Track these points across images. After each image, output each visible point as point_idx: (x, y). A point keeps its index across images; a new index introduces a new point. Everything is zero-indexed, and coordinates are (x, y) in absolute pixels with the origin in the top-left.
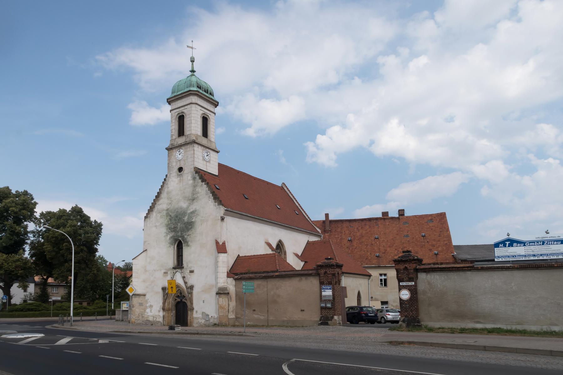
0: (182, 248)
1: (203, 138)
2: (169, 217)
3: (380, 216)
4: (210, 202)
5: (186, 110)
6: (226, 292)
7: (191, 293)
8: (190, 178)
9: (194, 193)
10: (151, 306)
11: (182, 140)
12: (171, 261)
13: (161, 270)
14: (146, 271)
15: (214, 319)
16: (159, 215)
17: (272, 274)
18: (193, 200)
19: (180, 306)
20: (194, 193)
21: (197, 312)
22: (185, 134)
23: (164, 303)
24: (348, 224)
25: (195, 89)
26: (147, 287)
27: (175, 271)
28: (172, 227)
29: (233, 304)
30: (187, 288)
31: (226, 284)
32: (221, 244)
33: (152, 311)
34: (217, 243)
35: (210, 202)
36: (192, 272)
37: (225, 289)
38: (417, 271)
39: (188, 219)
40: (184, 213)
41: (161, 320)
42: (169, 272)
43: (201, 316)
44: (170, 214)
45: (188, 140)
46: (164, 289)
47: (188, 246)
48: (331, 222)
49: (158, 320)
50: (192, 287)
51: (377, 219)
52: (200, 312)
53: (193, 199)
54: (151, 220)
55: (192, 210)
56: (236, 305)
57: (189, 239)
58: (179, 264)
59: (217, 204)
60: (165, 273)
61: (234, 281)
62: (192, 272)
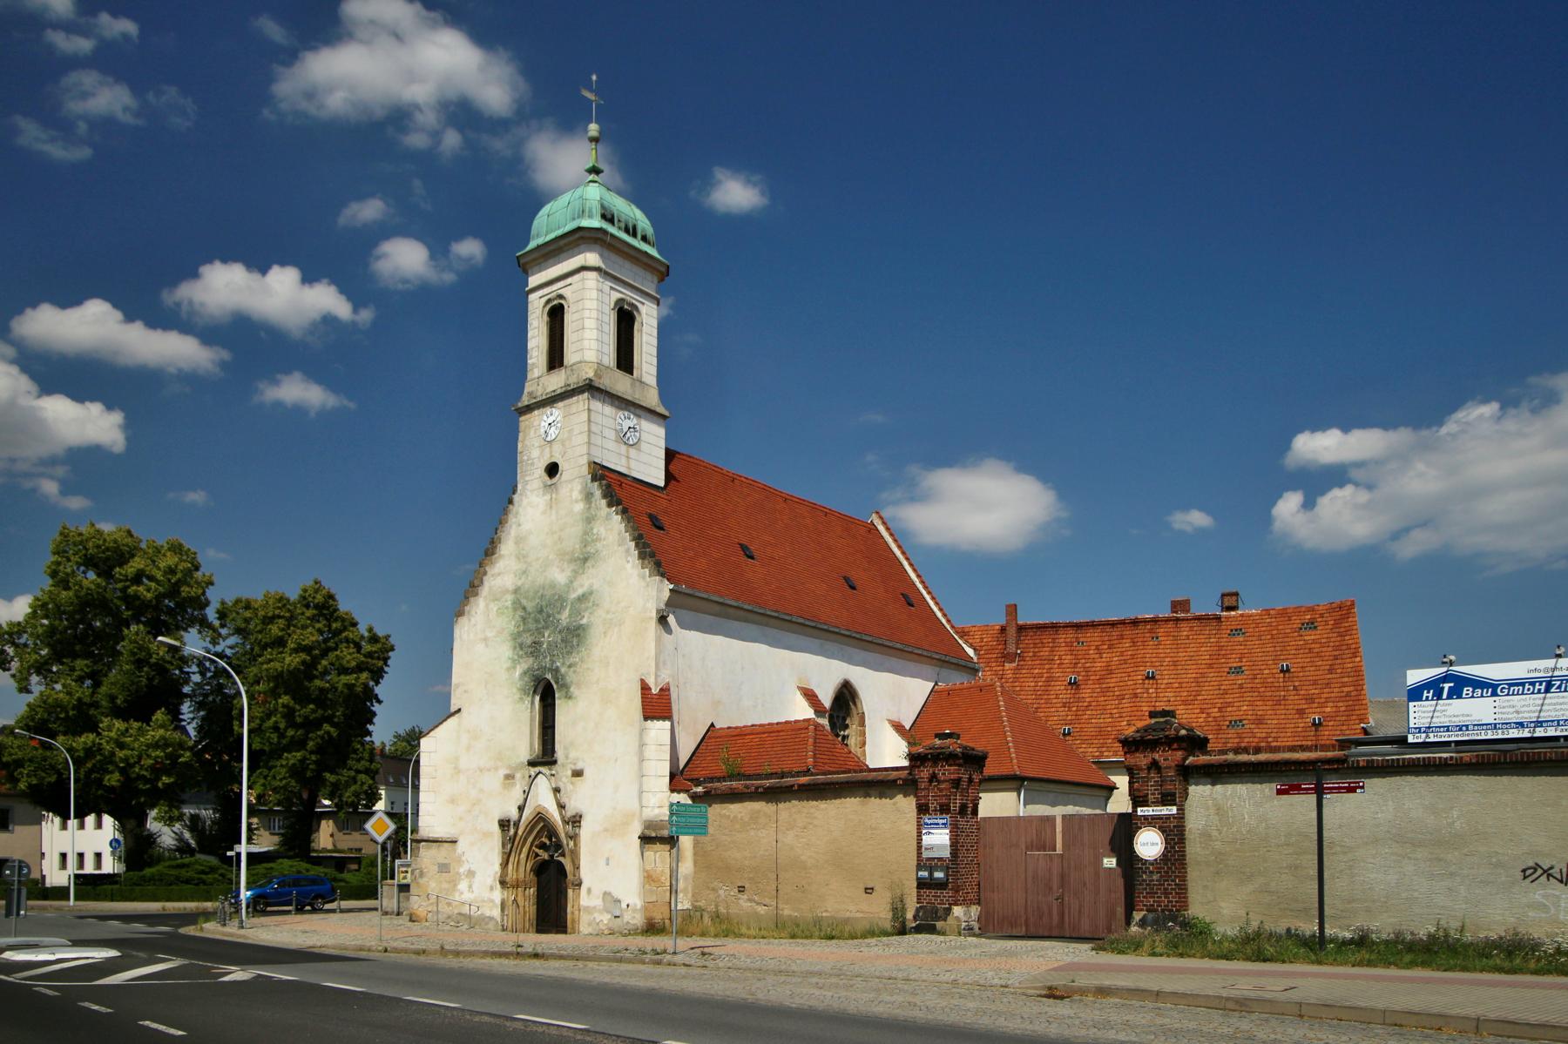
1: (620, 374)
4: (629, 566)
7: (574, 837)
8: (576, 494)
9: (587, 539)
10: (471, 874)
12: (525, 744)
13: (496, 769)
14: (457, 771)
15: (635, 911)
16: (494, 607)
18: (585, 560)
19: (545, 868)
20: (587, 539)
21: (589, 891)
22: (565, 362)
23: (505, 864)
24: (1071, 635)
25: (596, 223)
27: (533, 771)
28: (529, 641)
30: (566, 822)
32: (655, 691)
34: (645, 688)
35: (629, 566)
36: (578, 774)
38: (1188, 774)
42: (518, 776)
44: (524, 602)
46: (504, 824)
47: (569, 697)
48: (1021, 629)
50: (576, 820)
51: (1155, 621)
53: (584, 560)
55: (580, 591)
57: (571, 677)
58: (546, 756)
62: (578, 774)
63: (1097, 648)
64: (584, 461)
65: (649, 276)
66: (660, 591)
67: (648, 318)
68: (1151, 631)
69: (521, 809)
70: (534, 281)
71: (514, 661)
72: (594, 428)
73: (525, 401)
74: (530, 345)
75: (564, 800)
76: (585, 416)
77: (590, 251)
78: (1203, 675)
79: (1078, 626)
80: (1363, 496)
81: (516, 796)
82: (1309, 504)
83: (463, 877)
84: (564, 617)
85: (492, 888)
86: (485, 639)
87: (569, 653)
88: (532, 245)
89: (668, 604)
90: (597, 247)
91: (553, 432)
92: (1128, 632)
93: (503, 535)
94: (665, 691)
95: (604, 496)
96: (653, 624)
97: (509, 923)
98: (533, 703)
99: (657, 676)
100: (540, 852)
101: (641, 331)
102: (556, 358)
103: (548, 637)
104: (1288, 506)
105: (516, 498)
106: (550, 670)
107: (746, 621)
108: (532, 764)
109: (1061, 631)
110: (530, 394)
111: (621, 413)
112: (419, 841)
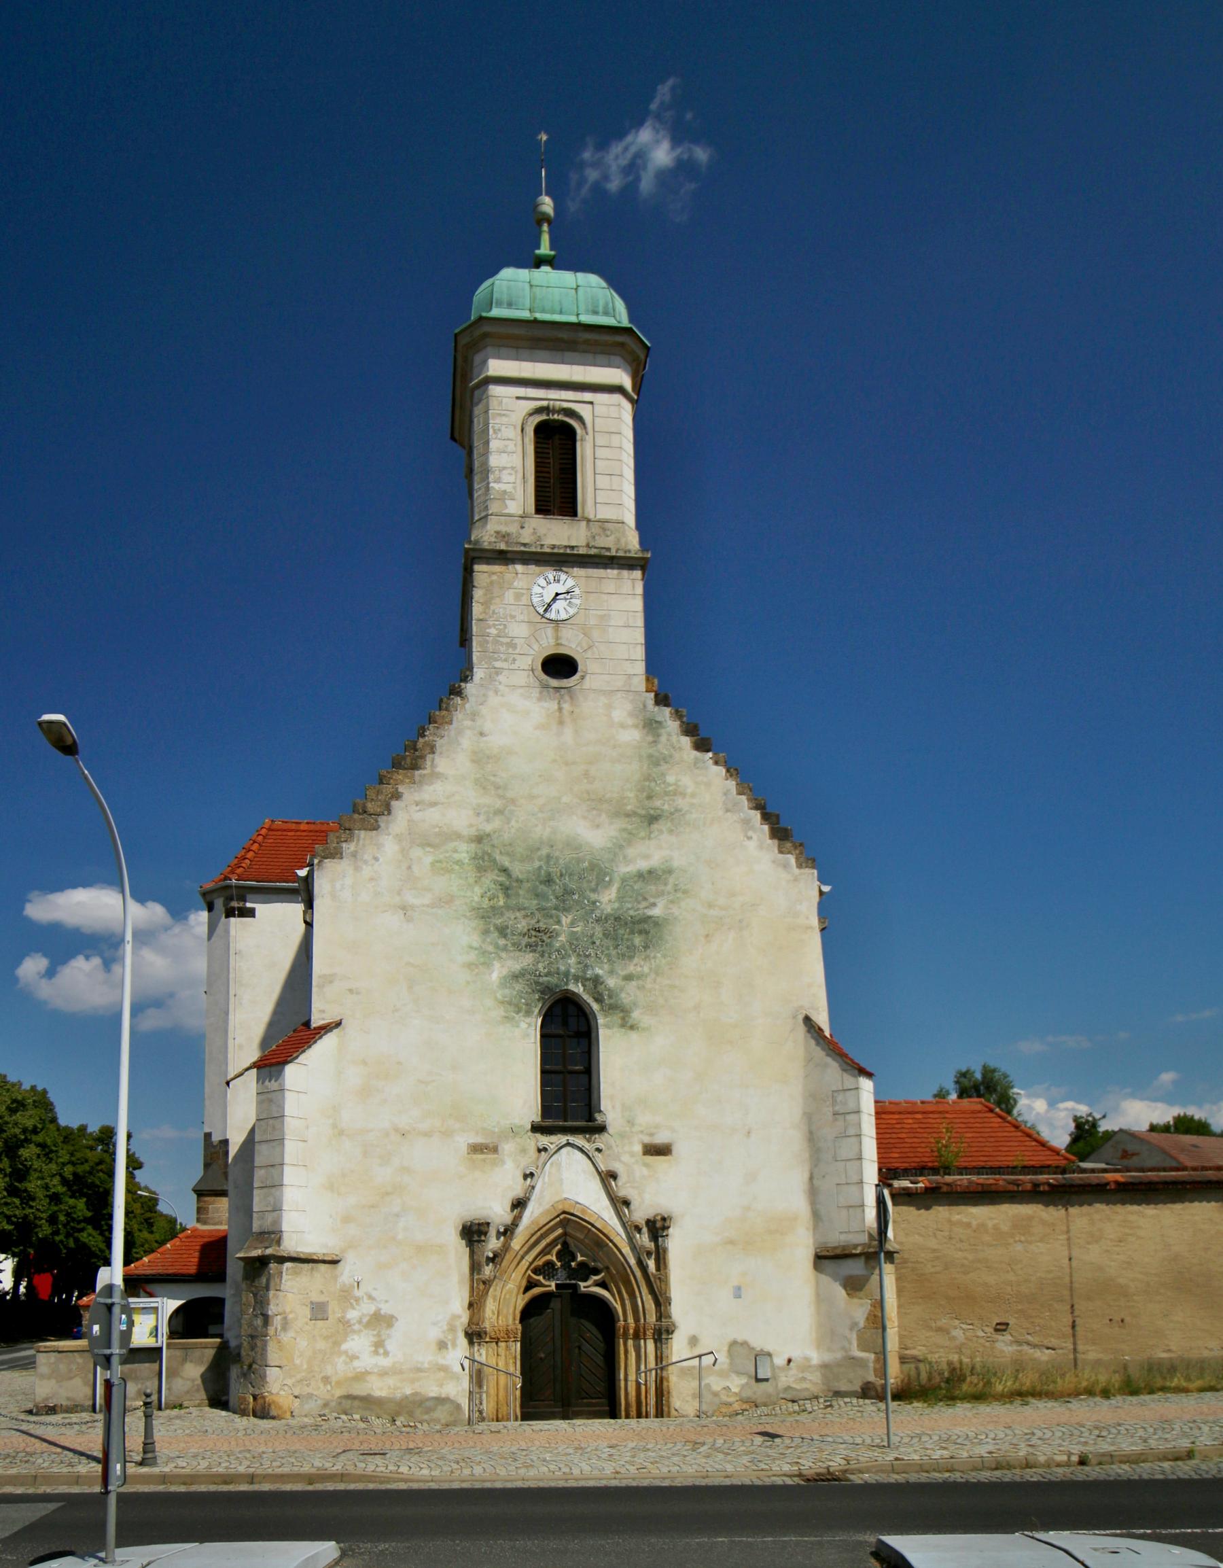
4: (752, 845)
7: (660, 1256)
8: (622, 711)
10: (380, 1321)
11: (557, 533)
13: (447, 1134)
15: (806, 1366)
16: (424, 859)
18: (652, 819)
19: (576, 1323)
23: (474, 1305)
26: (347, 1220)
27: (544, 1140)
28: (523, 925)
30: (632, 1229)
33: (391, 1345)
35: (752, 845)
36: (659, 1150)
39: (620, 899)
40: (598, 874)
41: (458, 1389)
42: (507, 1147)
46: (473, 1233)
47: (628, 1025)
49: (432, 1390)
50: (658, 1228)
54: (367, 871)
55: (643, 865)
58: (570, 1098)
59: (792, 859)
60: (484, 1149)
62: (659, 1150)
69: (519, 1204)
75: (623, 1188)
83: (383, 1331)
84: (608, 899)
85: (442, 1345)
86: (404, 908)
91: (561, 609)
97: (488, 1407)
103: (566, 926)
104: (32, 967)
105: (469, 688)
112: (282, 1260)
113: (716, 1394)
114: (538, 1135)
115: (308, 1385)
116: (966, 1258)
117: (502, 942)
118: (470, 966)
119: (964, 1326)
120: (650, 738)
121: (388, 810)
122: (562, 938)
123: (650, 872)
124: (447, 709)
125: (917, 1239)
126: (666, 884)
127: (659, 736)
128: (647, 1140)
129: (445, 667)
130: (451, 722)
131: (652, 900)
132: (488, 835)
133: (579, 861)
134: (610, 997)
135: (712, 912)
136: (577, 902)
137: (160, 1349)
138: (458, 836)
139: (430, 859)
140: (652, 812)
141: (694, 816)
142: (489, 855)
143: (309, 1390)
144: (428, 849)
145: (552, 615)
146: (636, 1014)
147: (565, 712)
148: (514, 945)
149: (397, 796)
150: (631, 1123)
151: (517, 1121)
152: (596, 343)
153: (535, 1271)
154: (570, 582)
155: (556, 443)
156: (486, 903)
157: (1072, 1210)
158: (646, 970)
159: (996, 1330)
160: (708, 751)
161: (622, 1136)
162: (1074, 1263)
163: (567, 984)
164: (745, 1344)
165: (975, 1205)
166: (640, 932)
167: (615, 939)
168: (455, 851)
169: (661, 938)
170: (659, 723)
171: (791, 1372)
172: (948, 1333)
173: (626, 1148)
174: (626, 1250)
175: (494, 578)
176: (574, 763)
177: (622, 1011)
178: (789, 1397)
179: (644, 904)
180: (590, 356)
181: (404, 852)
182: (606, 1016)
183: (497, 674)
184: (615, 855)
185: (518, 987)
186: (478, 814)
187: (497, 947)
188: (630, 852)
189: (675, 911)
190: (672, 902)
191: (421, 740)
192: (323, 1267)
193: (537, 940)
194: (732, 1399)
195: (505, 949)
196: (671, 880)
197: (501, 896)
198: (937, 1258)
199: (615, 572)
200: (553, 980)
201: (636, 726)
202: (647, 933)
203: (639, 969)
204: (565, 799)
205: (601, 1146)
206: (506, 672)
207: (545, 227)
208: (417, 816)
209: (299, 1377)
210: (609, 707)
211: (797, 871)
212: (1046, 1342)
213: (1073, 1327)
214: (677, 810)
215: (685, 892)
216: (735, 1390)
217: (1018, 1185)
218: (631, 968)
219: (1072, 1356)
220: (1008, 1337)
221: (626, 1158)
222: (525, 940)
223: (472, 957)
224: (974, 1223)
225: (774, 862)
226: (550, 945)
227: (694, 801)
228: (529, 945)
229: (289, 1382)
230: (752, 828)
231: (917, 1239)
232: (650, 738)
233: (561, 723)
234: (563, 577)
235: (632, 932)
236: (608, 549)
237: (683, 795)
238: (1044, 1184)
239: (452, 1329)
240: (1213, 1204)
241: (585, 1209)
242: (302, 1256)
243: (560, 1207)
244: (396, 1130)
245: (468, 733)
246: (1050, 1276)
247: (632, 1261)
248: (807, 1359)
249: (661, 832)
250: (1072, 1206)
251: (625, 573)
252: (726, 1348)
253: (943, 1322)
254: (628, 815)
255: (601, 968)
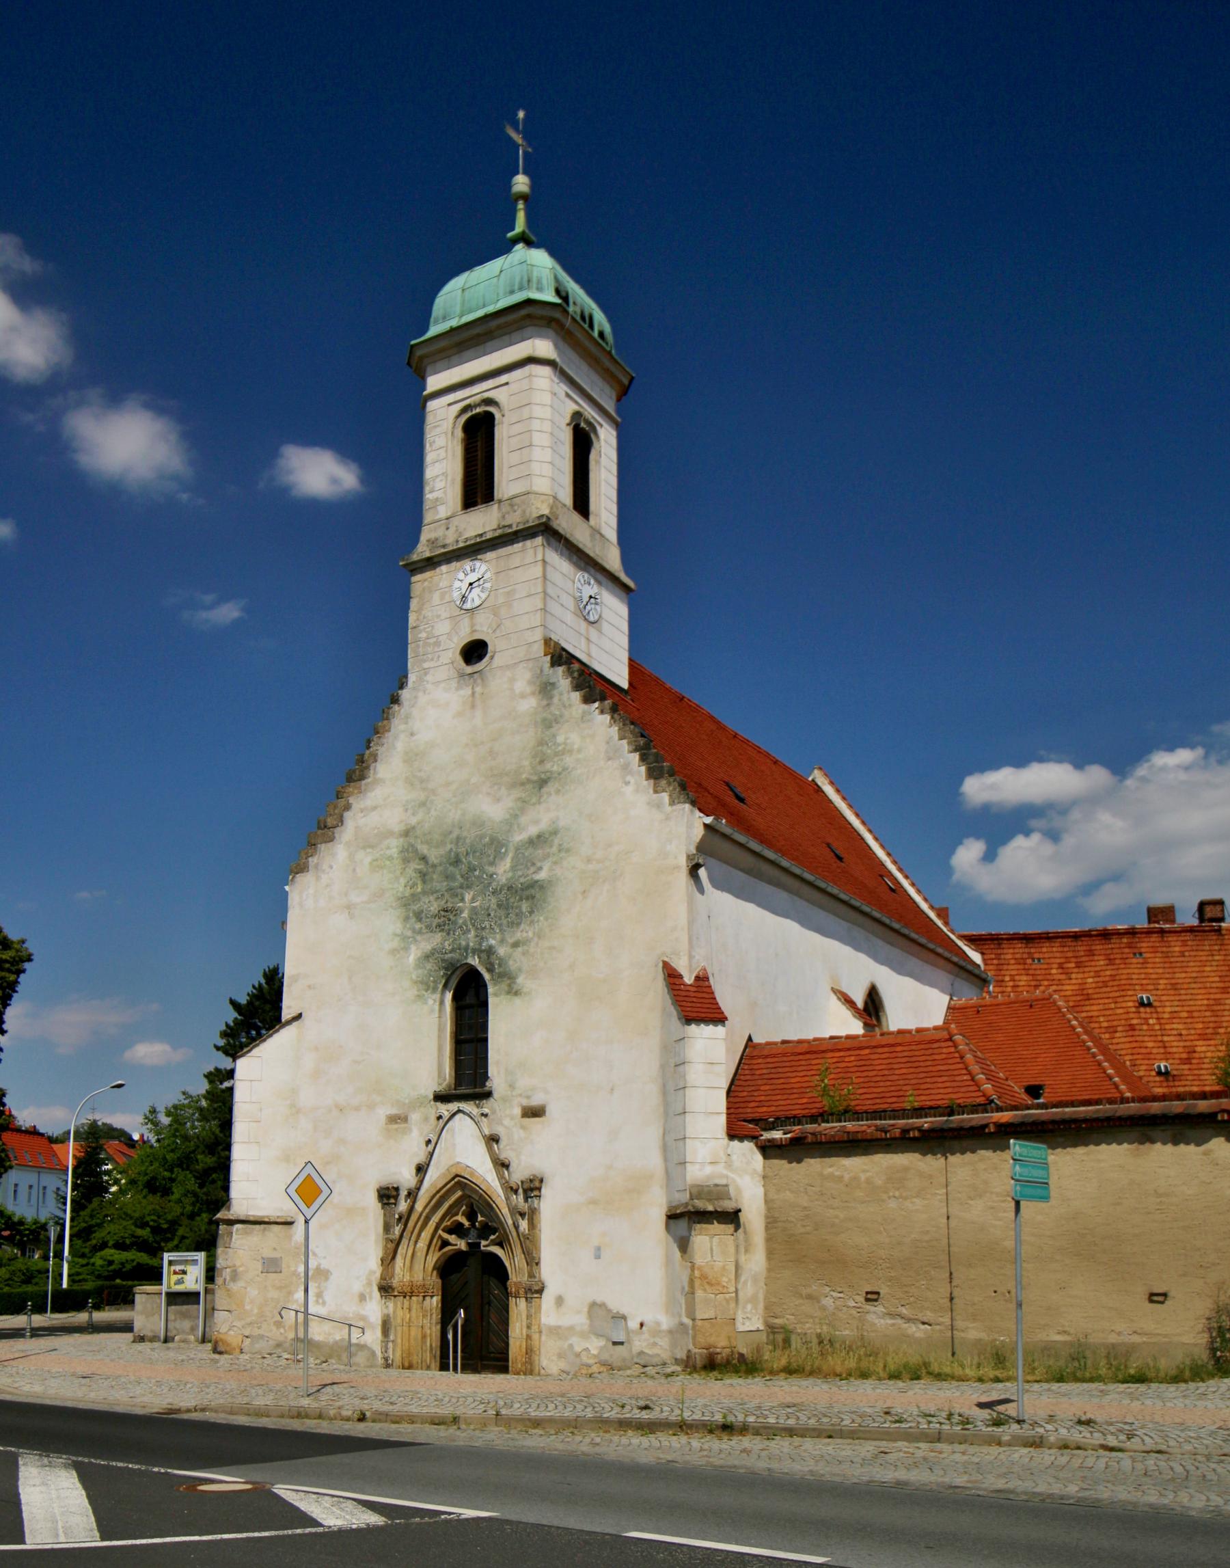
0: (485, 1004)
1: (576, 517)
2: (417, 865)
3: (1142, 923)
5: (504, 393)
6: (729, 1206)
7: (532, 1215)
11: (483, 522)
12: (427, 1056)
13: (371, 1107)
14: (296, 1110)
15: (656, 1332)
16: (365, 858)
17: (976, 1118)
18: (543, 783)
19: (472, 1277)
21: (560, 1301)
22: (497, 495)
23: (388, 1260)
24: (1020, 949)
27: (445, 1109)
28: (434, 907)
29: (756, 1261)
31: (720, 1169)
32: (689, 979)
33: (327, 1297)
34: (672, 976)
35: (629, 790)
36: (535, 1112)
37: (721, 1192)
40: (497, 846)
42: (415, 1117)
43: (580, 1320)
44: (423, 849)
45: (515, 520)
46: (387, 1195)
47: (514, 992)
50: (532, 1188)
51: (1132, 932)
52: (578, 1298)
54: (325, 879)
55: (533, 831)
56: (769, 1270)
57: (516, 960)
58: (469, 1077)
59: (665, 797)
61: (758, 1157)
62: (535, 1112)
63: (1061, 966)
64: (538, 635)
65: (608, 389)
66: (690, 826)
67: (606, 442)
68: (1129, 946)
69: (421, 1170)
70: (434, 382)
71: (404, 938)
72: (550, 591)
73: (423, 550)
74: (430, 473)
75: (505, 1153)
76: (537, 570)
77: (540, 336)
78: (1218, 1002)
79: (1027, 939)
80: (1048, 848)
81: (412, 1148)
82: (990, 856)
83: (308, 1282)
84: (503, 870)
85: (362, 1298)
86: (349, 907)
87: (514, 924)
88: (433, 331)
89: (701, 848)
90: (551, 332)
91: (475, 597)
92: (1098, 947)
93: (381, 751)
94: (702, 979)
95: (577, 687)
96: (683, 876)
97: (396, 1355)
98: (442, 1002)
99: (691, 957)
100: (452, 1238)
101: (598, 462)
102: (478, 485)
103: (469, 901)
104: (968, 854)
105: (405, 694)
106: (477, 951)
107: (778, 885)
108: (440, 1098)
109: (1005, 944)
110: (432, 543)
111: (579, 574)
112: (231, 1223)
113: (578, 1355)
114: (438, 1104)
115: (259, 1328)
116: (837, 1217)
117: (418, 926)
118: (393, 952)
119: (835, 1294)
120: (545, 702)
121: (341, 821)
122: (465, 915)
123: (539, 836)
124: (387, 719)
125: (788, 1195)
126: (551, 847)
127: (551, 697)
128: (525, 1102)
129: (382, 679)
130: (389, 730)
131: (539, 864)
132: (414, 828)
133: (482, 837)
134: (500, 965)
135: (591, 867)
136: (478, 877)
137: (198, 1294)
138: (390, 834)
139: (369, 859)
140: (543, 776)
141: (579, 771)
142: (412, 846)
143: (261, 1332)
144: (369, 850)
145: (468, 605)
146: (520, 980)
147: (477, 695)
148: (427, 927)
149: (348, 807)
150: (512, 1086)
151: (423, 1092)
152: (507, 325)
153: (450, 1231)
154: (484, 567)
155: (479, 432)
156: (408, 892)
157: (951, 1158)
158: (530, 934)
159: (867, 1300)
160: (594, 702)
161: (505, 1099)
162: (953, 1223)
163: (466, 958)
164: (603, 1305)
165: (848, 1155)
166: (527, 898)
167: (507, 909)
168: (388, 848)
169: (544, 901)
170: (553, 684)
171: (646, 1336)
172: (819, 1302)
173: (508, 1112)
174: (505, 1211)
175: (426, 584)
176: (482, 743)
177: (509, 978)
178: (642, 1362)
179: (532, 869)
180: (506, 338)
181: (351, 857)
182: (495, 985)
183: (426, 674)
184: (511, 825)
185: (429, 966)
186: (406, 810)
187: (414, 931)
188: (523, 820)
189: (558, 871)
190: (555, 863)
191: (368, 752)
192: (276, 1228)
193: (446, 919)
194: (591, 1361)
195: (420, 932)
196: (556, 842)
197: (419, 882)
198: (807, 1216)
199: (520, 544)
200: (456, 956)
201: (533, 693)
202: (533, 897)
203: (525, 935)
204: (474, 780)
205: (486, 1110)
206: (432, 671)
207: (521, 205)
208: (361, 822)
209: (249, 1320)
210: (512, 680)
211: (668, 809)
212: (920, 1316)
213: (952, 1299)
214: (565, 769)
215: (568, 851)
216: (595, 1352)
217: (886, 1132)
218: (519, 935)
219: (949, 1334)
220: (880, 1309)
221: (507, 1122)
222: (437, 921)
223: (396, 943)
224: (847, 1177)
225: (648, 804)
226: (455, 923)
227: (580, 756)
228: (439, 925)
229: (238, 1324)
230: (631, 773)
231: (788, 1195)
232: (545, 702)
233: (473, 706)
234: (478, 564)
235: (521, 900)
236: (510, 526)
237: (571, 752)
238: (913, 1129)
239: (369, 1284)
240: (1125, 1145)
241: (473, 1172)
242: (252, 1219)
243: (454, 1171)
244: (337, 1106)
245: (402, 736)
246: (926, 1238)
247: (510, 1222)
248: (658, 1324)
249: (549, 794)
250: (953, 1154)
251: (528, 543)
252: (586, 1310)
253: (814, 1288)
254: (522, 784)
255: (494, 939)
